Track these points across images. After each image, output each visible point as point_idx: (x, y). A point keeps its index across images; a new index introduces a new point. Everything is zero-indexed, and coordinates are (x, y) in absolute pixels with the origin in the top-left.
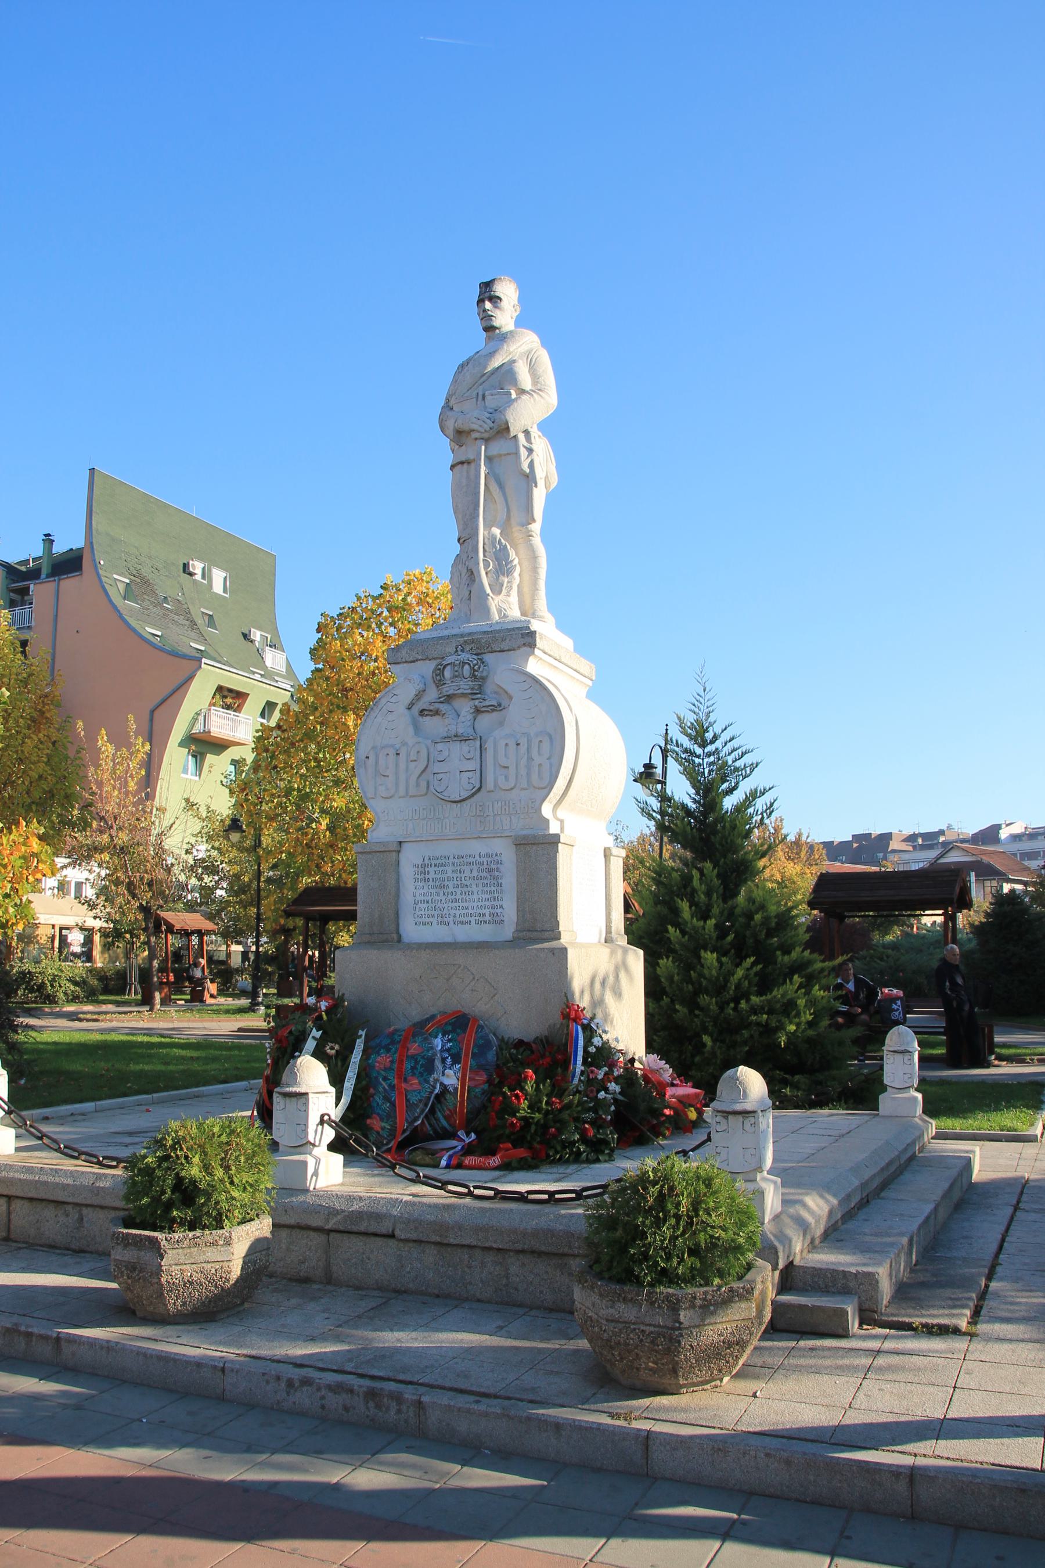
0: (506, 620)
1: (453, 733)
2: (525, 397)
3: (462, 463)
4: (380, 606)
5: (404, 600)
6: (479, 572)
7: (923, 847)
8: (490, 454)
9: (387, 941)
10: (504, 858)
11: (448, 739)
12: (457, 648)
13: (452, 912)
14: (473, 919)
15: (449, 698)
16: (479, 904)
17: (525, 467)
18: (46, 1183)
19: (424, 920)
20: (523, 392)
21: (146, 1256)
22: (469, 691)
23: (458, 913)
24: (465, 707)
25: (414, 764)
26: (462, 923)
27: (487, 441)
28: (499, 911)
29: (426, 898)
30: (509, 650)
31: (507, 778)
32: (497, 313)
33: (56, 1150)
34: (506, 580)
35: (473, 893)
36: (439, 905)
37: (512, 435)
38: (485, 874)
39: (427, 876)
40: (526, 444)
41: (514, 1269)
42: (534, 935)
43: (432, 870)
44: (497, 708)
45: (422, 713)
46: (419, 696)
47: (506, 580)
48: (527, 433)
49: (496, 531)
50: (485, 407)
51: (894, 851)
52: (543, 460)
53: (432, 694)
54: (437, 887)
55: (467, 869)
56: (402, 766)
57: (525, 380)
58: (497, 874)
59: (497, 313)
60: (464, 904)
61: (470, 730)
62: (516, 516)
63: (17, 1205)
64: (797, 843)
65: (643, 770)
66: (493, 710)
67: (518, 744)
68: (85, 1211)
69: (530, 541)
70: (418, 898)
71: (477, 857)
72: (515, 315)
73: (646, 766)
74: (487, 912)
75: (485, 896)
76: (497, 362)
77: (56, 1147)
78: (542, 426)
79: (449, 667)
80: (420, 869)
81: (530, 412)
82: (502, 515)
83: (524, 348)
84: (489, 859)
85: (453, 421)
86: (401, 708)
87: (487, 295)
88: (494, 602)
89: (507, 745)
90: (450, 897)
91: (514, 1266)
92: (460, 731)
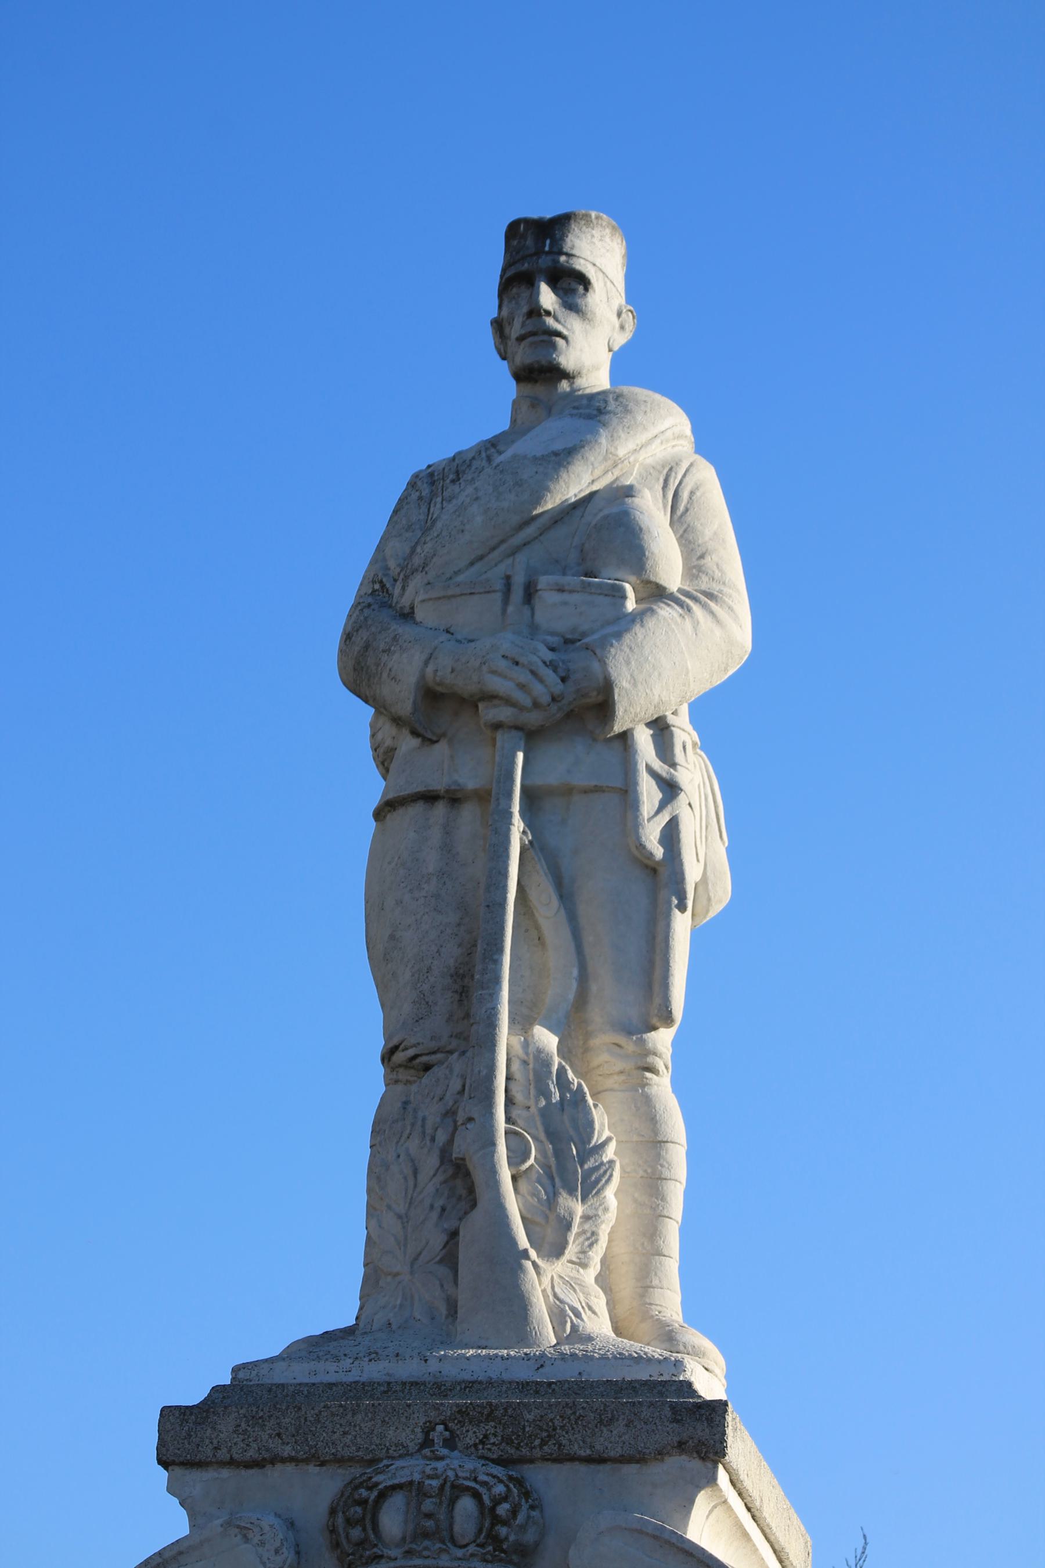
0: (578, 1349)
2: (666, 612)
3: (430, 798)
6: (493, 1171)
8: (538, 781)
17: (652, 836)
20: (655, 593)
27: (533, 738)
32: (572, 326)
34: (579, 1209)
37: (618, 728)
40: (658, 765)
47: (579, 1209)
48: (661, 728)
49: (548, 1039)
50: (534, 629)
52: (700, 825)
57: (669, 565)
59: (572, 326)
62: (609, 995)
69: (644, 1084)
72: (621, 340)
76: (576, 483)
78: (702, 710)
79: (397, 1501)
81: (676, 665)
82: (560, 988)
83: (656, 453)
85: (418, 658)
87: (544, 262)
88: (544, 1281)
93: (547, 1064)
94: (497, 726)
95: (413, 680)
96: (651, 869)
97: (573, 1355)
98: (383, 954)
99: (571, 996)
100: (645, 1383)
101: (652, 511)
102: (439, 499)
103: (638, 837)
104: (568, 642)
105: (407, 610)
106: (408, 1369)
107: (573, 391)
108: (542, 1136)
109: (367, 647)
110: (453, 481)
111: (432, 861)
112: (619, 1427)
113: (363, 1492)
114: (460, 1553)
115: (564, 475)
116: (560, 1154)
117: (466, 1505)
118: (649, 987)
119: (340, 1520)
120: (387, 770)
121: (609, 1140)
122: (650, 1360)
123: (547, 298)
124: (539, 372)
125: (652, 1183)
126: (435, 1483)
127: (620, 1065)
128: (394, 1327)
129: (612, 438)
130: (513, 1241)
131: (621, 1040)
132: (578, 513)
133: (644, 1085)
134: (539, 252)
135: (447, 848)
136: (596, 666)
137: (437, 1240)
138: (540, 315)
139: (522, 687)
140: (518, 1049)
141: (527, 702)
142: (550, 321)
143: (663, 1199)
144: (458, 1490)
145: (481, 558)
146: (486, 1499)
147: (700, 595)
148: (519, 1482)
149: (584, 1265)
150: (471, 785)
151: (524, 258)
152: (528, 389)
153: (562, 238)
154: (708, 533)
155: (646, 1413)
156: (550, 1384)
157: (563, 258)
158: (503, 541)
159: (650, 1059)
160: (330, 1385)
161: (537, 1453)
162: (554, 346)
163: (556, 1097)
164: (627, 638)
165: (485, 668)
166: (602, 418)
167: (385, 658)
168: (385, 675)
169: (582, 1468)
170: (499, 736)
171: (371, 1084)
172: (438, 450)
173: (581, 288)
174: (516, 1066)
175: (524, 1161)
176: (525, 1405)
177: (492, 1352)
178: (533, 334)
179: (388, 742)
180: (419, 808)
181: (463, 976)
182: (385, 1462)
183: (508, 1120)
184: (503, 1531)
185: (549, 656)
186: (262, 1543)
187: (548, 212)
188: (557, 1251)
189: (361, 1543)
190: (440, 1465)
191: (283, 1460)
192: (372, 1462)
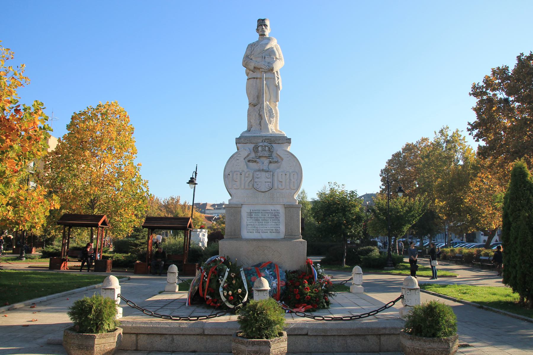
3: (254, 78)
4: (97, 112)
5: (107, 111)
7: (217, 209)
9: (237, 238)
10: (280, 211)
11: (259, 170)
18: (157, 327)
20: (277, 58)
21: (263, 348)
24: (266, 161)
25: (247, 178)
27: (265, 72)
33: (150, 315)
41: (349, 341)
42: (292, 237)
43: (253, 214)
44: (276, 162)
45: (249, 161)
46: (248, 156)
48: (277, 72)
49: (268, 103)
51: (208, 209)
52: (280, 81)
53: (253, 155)
55: (267, 214)
56: (243, 178)
63: (141, 337)
64: (184, 205)
68: (175, 337)
73: (191, 178)
76: (268, 47)
77: (151, 314)
78: (280, 70)
81: (278, 66)
86: (242, 159)
91: (349, 340)
92: (264, 169)
96: (276, 86)
101: (275, 49)
106: (258, 135)
111: (254, 85)
123: (264, 27)
124: (262, 35)
135: (256, 83)
147: (280, 59)
150: (259, 77)
171: (247, 106)
172: (251, 42)
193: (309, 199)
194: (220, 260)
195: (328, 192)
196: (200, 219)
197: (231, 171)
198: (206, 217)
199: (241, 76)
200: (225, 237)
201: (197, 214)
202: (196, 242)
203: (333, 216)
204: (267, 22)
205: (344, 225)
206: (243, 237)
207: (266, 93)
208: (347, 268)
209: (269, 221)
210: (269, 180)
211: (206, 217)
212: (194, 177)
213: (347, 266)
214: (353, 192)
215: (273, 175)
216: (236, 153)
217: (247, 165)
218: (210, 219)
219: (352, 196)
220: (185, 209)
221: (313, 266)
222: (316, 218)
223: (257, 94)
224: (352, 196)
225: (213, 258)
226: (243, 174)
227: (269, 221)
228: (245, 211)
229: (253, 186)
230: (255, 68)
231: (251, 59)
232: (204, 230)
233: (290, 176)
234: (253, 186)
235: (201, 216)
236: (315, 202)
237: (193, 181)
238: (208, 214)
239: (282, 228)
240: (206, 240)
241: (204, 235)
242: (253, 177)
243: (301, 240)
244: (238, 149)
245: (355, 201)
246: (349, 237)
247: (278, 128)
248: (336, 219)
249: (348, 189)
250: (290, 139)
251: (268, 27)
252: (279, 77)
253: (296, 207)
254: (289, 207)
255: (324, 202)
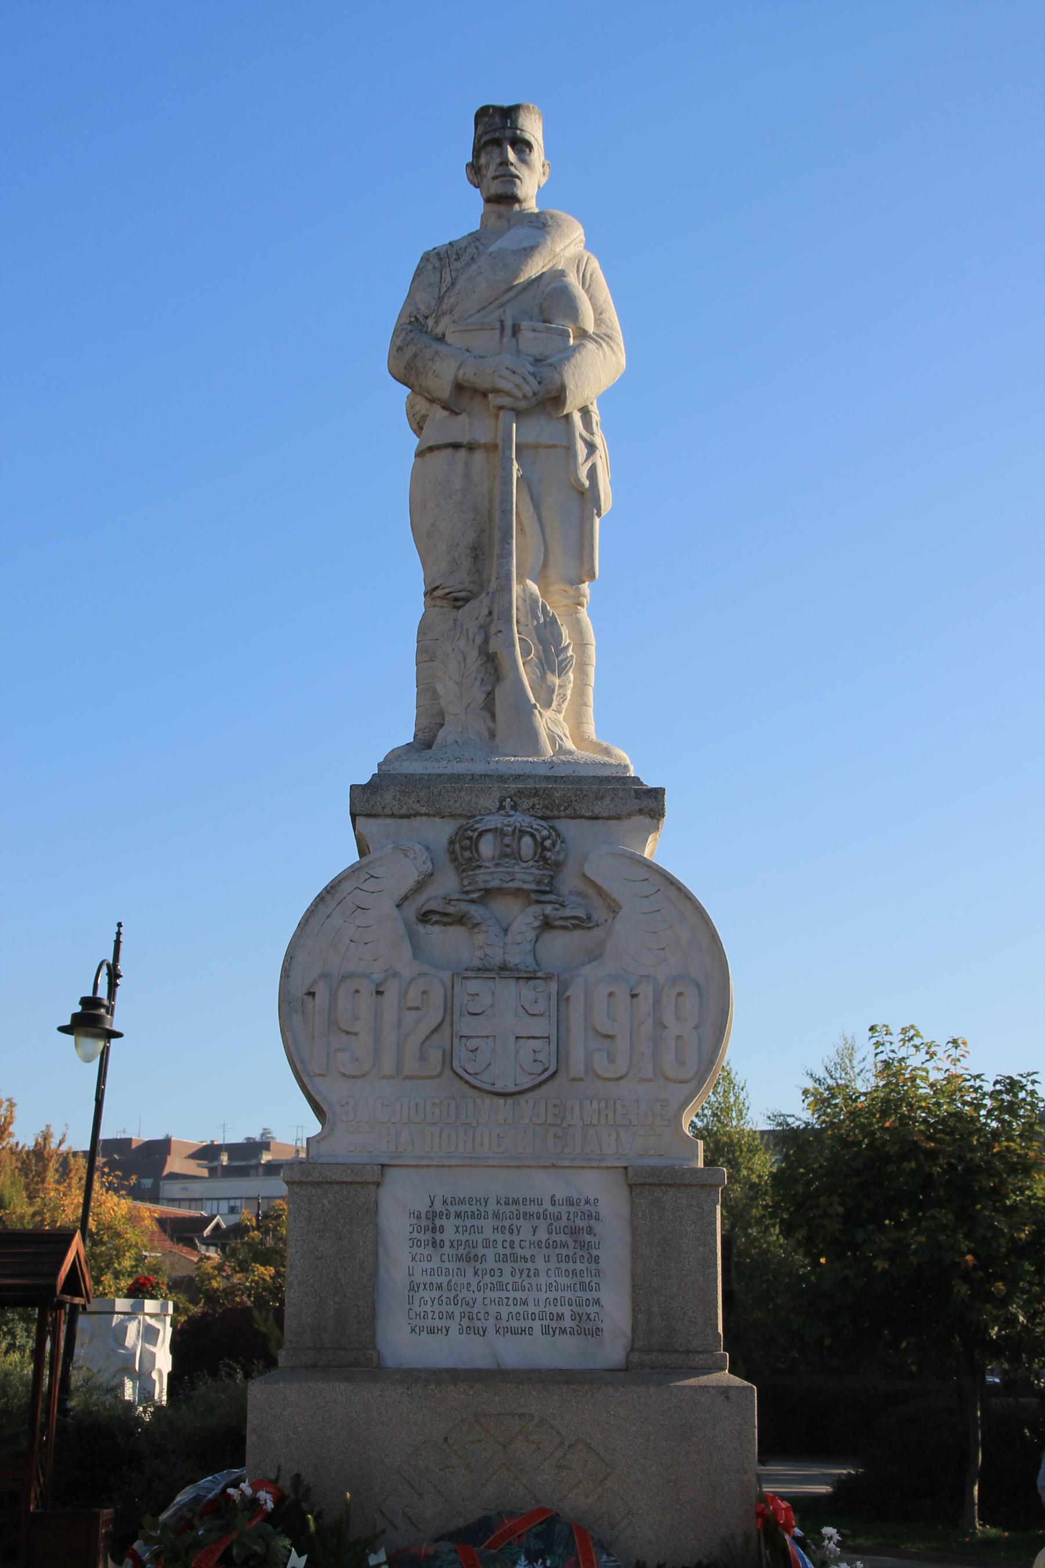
1: (497, 961)
3: (456, 446)
6: (515, 661)
7: (230, 1172)
12: (502, 800)
13: (493, 1309)
14: (537, 1325)
15: (488, 894)
16: (551, 1295)
19: (430, 1322)
20: (583, 334)
22: (533, 887)
23: (504, 1311)
24: (523, 920)
25: (410, 1017)
26: (514, 1332)
27: (519, 414)
28: (592, 1310)
29: (437, 1279)
30: (609, 818)
31: (611, 1059)
34: (557, 682)
35: (537, 1273)
36: (464, 1293)
37: (565, 412)
38: (564, 1238)
39: (439, 1237)
40: (585, 433)
44: (582, 923)
45: (425, 917)
46: (420, 886)
47: (557, 682)
48: (585, 412)
49: (534, 587)
50: (518, 352)
51: (174, 1176)
52: (602, 466)
53: (448, 883)
54: (459, 1259)
55: (526, 1226)
58: (588, 1238)
60: (519, 1295)
61: (530, 961)
64: (39, 1153)
65: (78, 1009)
66: (576, 927)
67: (634, 996)
69: (576, 612)
70: (418, 1278)
71: (547, 1204)
73: (85, 1002)
74: (567, 1311)
75: (563, 1280)
76: (535, 268)
78: (602, 399)
79: (489, 837)
80: (424, 1222)
81: (595, 375)
84: (573, 1209)
86: (387, 906)
87: (508, 133)
89: (611, 994)
90: (488, 1279)
92: (513, 960)
93: (537, 602)
94: (501, 408)
95: (451, 378)
96: (581, 493)
97: (569, 761)
98: (424, 536)
99: (541, 563)
100: (614, 778)
102: (448, 270)
103: (577, 475)
104: (537, 360)
105: (440, 336)
106: (479, 768)
107: (522, 211)
108: (536, 641)
109: (415, 356)
110: (456, 260)
111: (458, 483)
112: (607, 801)
113: (471, 833)
114: (525, 865)
115: (530, 262)
116: (546, 651)
117: (527, 840)
118: (581, 559)
119: (457, 847)
120: (421, 428)
121: (569, 645)
122: (611, 765)
123: (511, 156)
124: (503, 198)
125: (582, 669)
126: (510, 829)
127: (565, 602)
128: (460, 743)
129: (553, 242)
130: (529, 700)
131: (567, 588)
132: (536, 284)
133: (576, 613)
134: (504, 127)
135: (467, 475)
136: (557, 376)
137: (480, 697)
138: (507, 165)
139: (517, 386)
140: (520, 592)
141: (520, 395)
142: (512, 169)
143: (587, 675)
144: (522, 833)
145: (484, 308)
146: (538, 837)
147: (603, 338)
148: (555, 829)
149: (560, 712)
151: (495, 130)
152: (493, 207)
153: (516, 119)
154: (602, 299)
155: (621, 794)
156: (562, 777)
157: (518, 132)
158: (496, 299)
159: (582, 599)
160: (440, 775)
161: (563, 814)
162: (514, 184)
163: (542, 620)
164: (573, 360)
165: (496, 374)
166: (548, 229)
167: (430, 364)
168: (430, 374)
169: (587, 822)
170: (502, 413)
171: (415, 606)
172: (441, 240)
173: (528, 150)
174: (520, 602)
175: (529, 655)
176: (556, 789)
177: (525, 759)
178: (503, 176)
179: (423, 412)
180: (450, 450)
181: (476, 549)
182: (478, 818)
183: (519, 633)
184: (548, 854)
185: (532, 369)
186: (416, 858)
187: (506, 103)
188: (548, 704)
189: (470, 860)
190: (512, 819)
191: (421, 815)
192: (470, 817)
193: (757, 1119)
194: (253, 1503)
195: (865, 1082)
196: (131, 1235)
197: (324, 976)
198: (162, 1222)
199: (381, 437)
200: (282, 1357)
201: (114, 1206)
202: (102, 1379)
203: (899, 1226)
204: (533, 127)
205: (966, 1276)
206: (390, 1363)
207: (521, 530)
208: (989, 1543)
209: (540, 1264)
210: (541, 1027)
211: (162, 1222)
212: (103, 993)
213: (992, 1531)
214: (1012, 1085)
215: (563, 998)
216: (352, 871)
217: (412, 935)
218: (183, 1231)
219: (1012, 1109)
220: (41, 1175)
221: (798, 1540)
222: (801, 1234)
223: (470, 536)
224: (1012, 1109)
225: (209, 1485)
226: (392, 990)
227: (540, 1264)
228: (399, 1206)
229: (448, 1058)
230: (460, 388)
231: (441, 339)
232: (150, 1305)
233: (657, 1002)
234: (448, 1058)
235: (133, 1219)
236: (787, 1139)
237: (98, 1020)
238: (172, 1201)
239: (615, 1309)
240: (164, 1361)
241: (150, 1334)
242: (448, 1008)
243: (725, 1377)
244: (362, 853)
245: (1028, 1133)
246: (996, 1349)
247: (591, 730)
248: (916, 1240)
249: (988, 1064)
250: (657, 794)
251: (538, 156)
252: (599, 440)
253: (697, 1185)
254: (652, 1187)
255: (844, 1143)
